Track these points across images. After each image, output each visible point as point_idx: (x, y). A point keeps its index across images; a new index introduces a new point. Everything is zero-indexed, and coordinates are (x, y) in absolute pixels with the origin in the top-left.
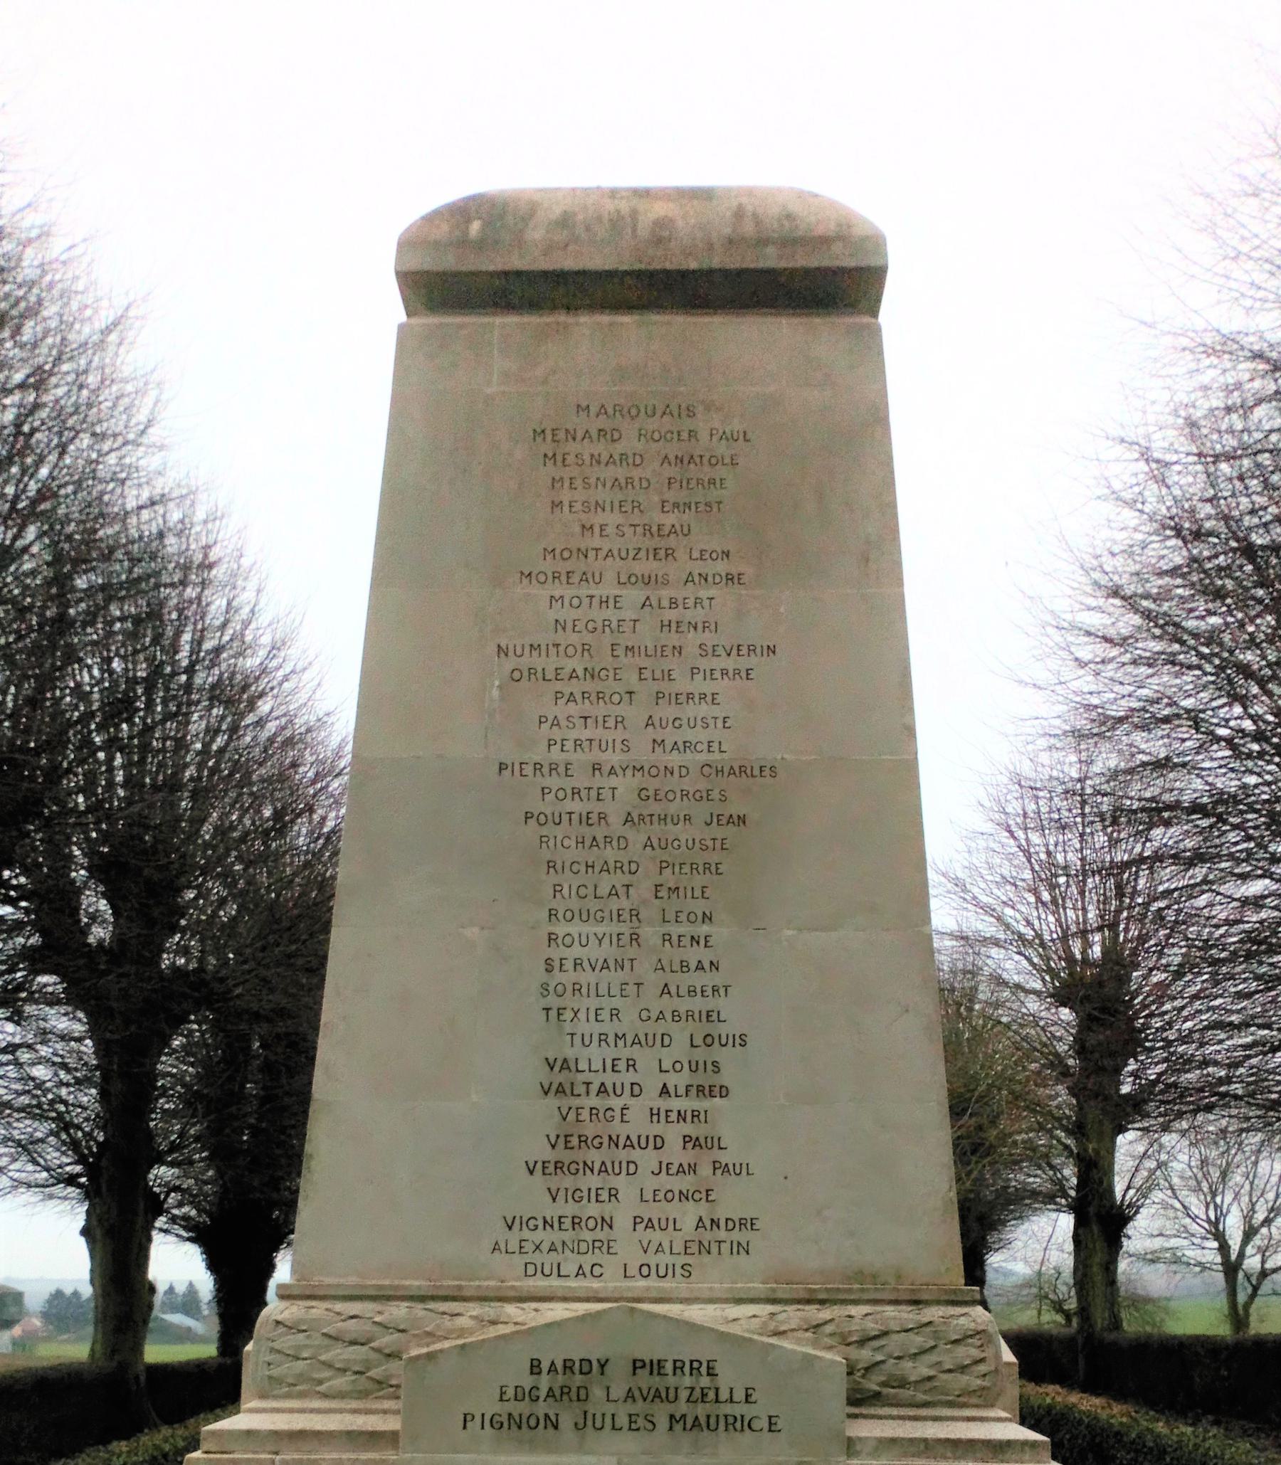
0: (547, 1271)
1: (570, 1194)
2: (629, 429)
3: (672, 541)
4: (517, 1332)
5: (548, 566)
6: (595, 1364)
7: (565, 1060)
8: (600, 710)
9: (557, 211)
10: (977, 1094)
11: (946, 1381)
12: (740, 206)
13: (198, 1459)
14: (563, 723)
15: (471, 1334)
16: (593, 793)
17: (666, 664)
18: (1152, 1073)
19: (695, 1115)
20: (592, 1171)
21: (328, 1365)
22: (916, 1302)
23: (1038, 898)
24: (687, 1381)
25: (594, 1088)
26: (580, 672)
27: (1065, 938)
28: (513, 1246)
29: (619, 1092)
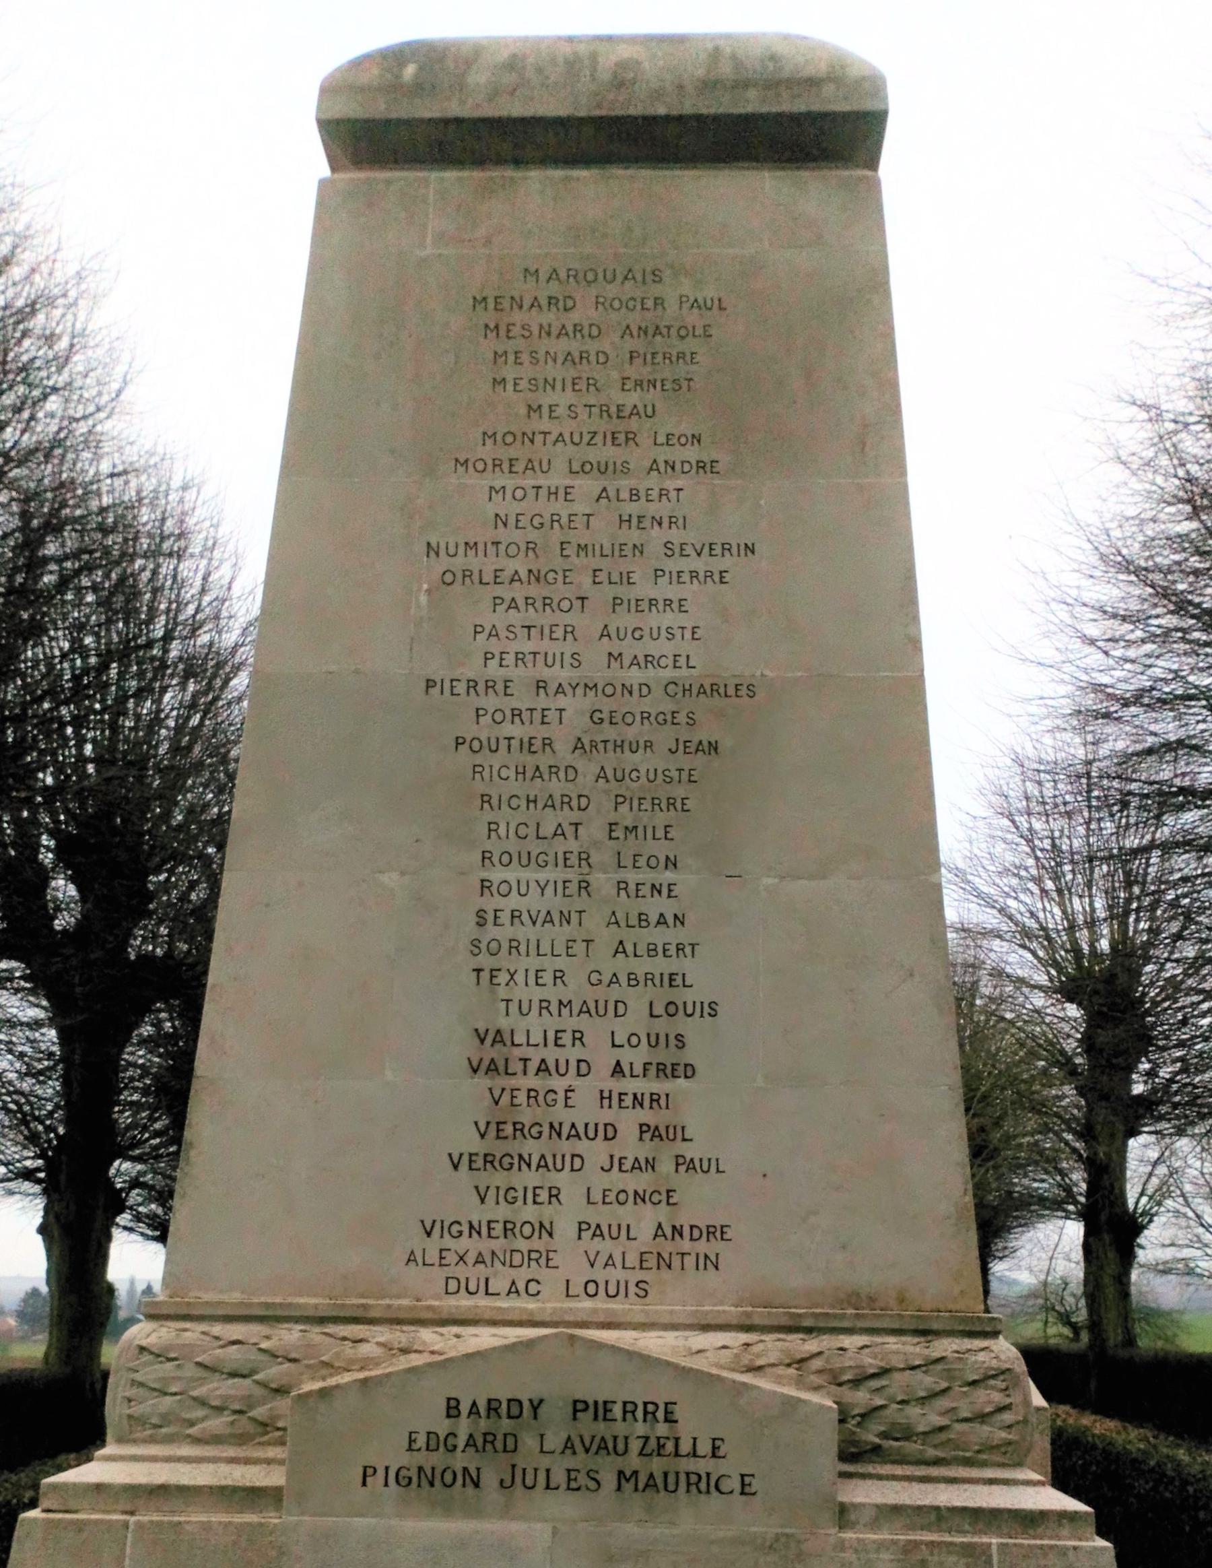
0: (472, 1288)
1: (502, 1193)
2: (585, 297)
3: (634, 424)
4: (430, 1365)
5: (487, 452)
6: (526, 1404)
7: (498, 1031)
8: (546, 618)
9: (505, 54)
10: (979, 1094)
11: (963, 1433)
12: (717, 49)
13: (35, 1520)
14: (503, 634)
15: (378, 1364)
16: (537, 716)
17: (624, 565)
18: (1165, 1073)
19: (655, 1099)
20: (529, 1165)
21: (202, 1402)
22: (924, 1333)
23: (1044, 892)
24: (640, 1428)
25: (533, 1066)
26: (523, 574)
27: (1072, 928)
28: (433, 1256)
29: (562, 1071)
